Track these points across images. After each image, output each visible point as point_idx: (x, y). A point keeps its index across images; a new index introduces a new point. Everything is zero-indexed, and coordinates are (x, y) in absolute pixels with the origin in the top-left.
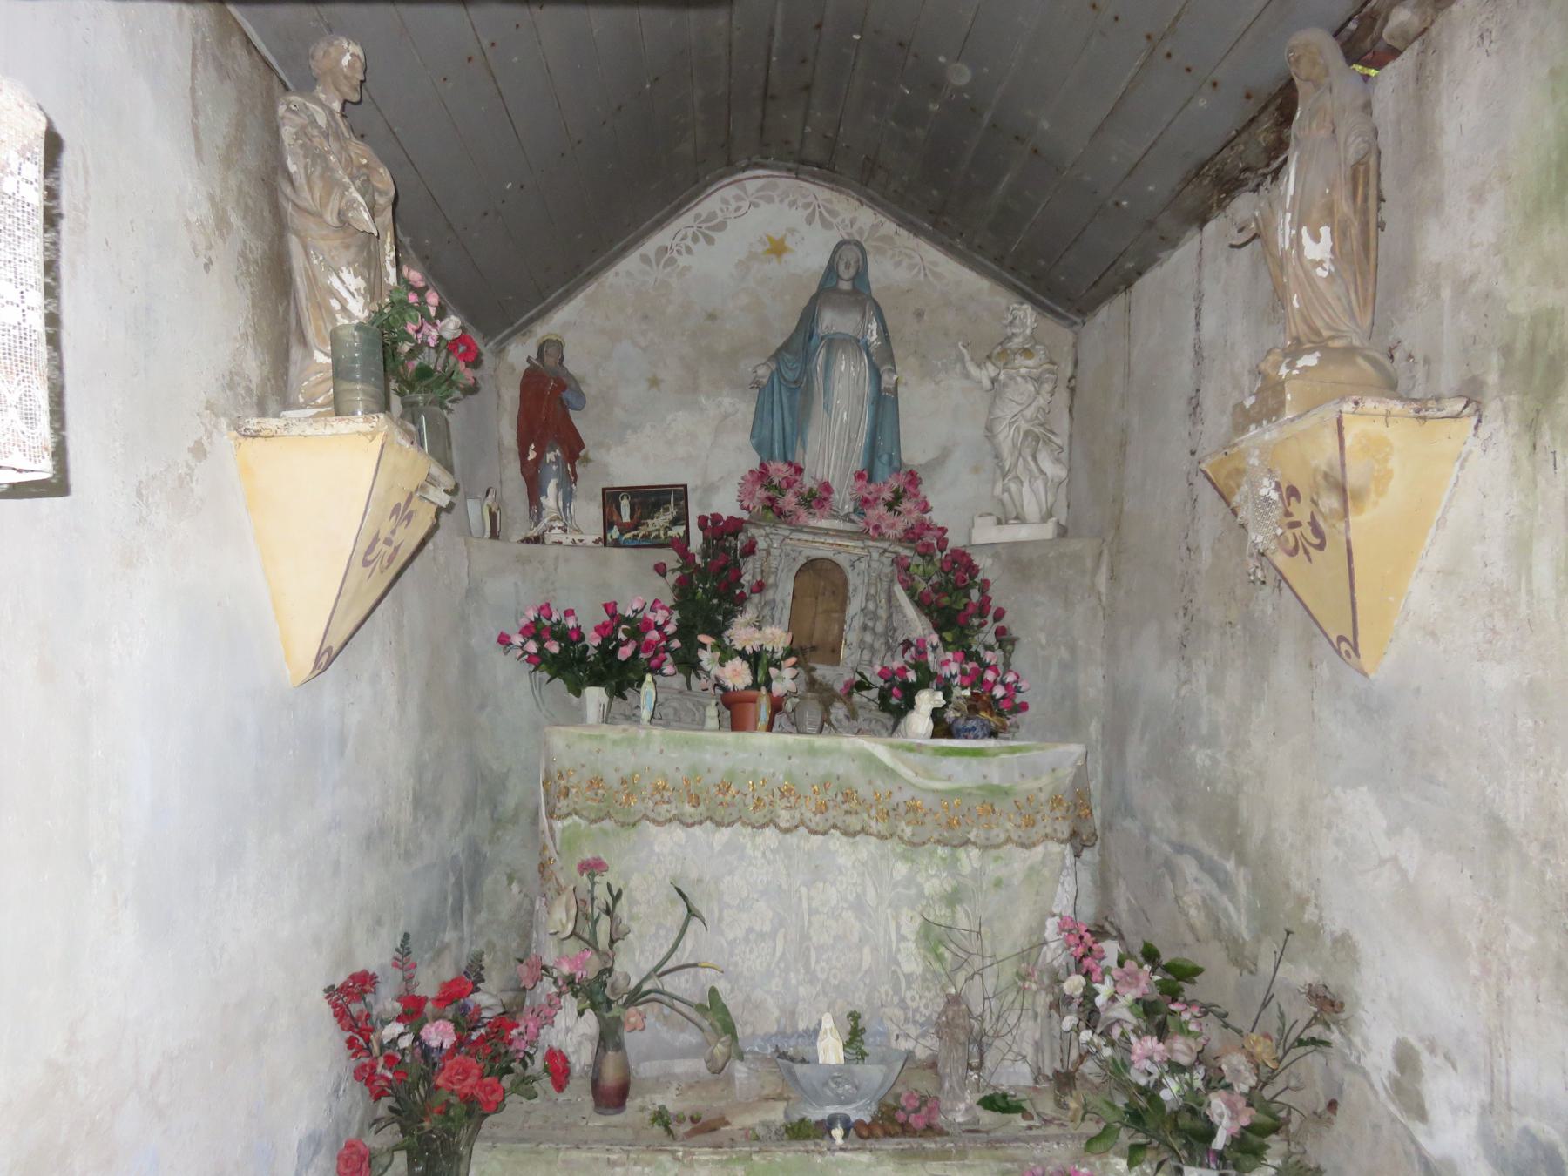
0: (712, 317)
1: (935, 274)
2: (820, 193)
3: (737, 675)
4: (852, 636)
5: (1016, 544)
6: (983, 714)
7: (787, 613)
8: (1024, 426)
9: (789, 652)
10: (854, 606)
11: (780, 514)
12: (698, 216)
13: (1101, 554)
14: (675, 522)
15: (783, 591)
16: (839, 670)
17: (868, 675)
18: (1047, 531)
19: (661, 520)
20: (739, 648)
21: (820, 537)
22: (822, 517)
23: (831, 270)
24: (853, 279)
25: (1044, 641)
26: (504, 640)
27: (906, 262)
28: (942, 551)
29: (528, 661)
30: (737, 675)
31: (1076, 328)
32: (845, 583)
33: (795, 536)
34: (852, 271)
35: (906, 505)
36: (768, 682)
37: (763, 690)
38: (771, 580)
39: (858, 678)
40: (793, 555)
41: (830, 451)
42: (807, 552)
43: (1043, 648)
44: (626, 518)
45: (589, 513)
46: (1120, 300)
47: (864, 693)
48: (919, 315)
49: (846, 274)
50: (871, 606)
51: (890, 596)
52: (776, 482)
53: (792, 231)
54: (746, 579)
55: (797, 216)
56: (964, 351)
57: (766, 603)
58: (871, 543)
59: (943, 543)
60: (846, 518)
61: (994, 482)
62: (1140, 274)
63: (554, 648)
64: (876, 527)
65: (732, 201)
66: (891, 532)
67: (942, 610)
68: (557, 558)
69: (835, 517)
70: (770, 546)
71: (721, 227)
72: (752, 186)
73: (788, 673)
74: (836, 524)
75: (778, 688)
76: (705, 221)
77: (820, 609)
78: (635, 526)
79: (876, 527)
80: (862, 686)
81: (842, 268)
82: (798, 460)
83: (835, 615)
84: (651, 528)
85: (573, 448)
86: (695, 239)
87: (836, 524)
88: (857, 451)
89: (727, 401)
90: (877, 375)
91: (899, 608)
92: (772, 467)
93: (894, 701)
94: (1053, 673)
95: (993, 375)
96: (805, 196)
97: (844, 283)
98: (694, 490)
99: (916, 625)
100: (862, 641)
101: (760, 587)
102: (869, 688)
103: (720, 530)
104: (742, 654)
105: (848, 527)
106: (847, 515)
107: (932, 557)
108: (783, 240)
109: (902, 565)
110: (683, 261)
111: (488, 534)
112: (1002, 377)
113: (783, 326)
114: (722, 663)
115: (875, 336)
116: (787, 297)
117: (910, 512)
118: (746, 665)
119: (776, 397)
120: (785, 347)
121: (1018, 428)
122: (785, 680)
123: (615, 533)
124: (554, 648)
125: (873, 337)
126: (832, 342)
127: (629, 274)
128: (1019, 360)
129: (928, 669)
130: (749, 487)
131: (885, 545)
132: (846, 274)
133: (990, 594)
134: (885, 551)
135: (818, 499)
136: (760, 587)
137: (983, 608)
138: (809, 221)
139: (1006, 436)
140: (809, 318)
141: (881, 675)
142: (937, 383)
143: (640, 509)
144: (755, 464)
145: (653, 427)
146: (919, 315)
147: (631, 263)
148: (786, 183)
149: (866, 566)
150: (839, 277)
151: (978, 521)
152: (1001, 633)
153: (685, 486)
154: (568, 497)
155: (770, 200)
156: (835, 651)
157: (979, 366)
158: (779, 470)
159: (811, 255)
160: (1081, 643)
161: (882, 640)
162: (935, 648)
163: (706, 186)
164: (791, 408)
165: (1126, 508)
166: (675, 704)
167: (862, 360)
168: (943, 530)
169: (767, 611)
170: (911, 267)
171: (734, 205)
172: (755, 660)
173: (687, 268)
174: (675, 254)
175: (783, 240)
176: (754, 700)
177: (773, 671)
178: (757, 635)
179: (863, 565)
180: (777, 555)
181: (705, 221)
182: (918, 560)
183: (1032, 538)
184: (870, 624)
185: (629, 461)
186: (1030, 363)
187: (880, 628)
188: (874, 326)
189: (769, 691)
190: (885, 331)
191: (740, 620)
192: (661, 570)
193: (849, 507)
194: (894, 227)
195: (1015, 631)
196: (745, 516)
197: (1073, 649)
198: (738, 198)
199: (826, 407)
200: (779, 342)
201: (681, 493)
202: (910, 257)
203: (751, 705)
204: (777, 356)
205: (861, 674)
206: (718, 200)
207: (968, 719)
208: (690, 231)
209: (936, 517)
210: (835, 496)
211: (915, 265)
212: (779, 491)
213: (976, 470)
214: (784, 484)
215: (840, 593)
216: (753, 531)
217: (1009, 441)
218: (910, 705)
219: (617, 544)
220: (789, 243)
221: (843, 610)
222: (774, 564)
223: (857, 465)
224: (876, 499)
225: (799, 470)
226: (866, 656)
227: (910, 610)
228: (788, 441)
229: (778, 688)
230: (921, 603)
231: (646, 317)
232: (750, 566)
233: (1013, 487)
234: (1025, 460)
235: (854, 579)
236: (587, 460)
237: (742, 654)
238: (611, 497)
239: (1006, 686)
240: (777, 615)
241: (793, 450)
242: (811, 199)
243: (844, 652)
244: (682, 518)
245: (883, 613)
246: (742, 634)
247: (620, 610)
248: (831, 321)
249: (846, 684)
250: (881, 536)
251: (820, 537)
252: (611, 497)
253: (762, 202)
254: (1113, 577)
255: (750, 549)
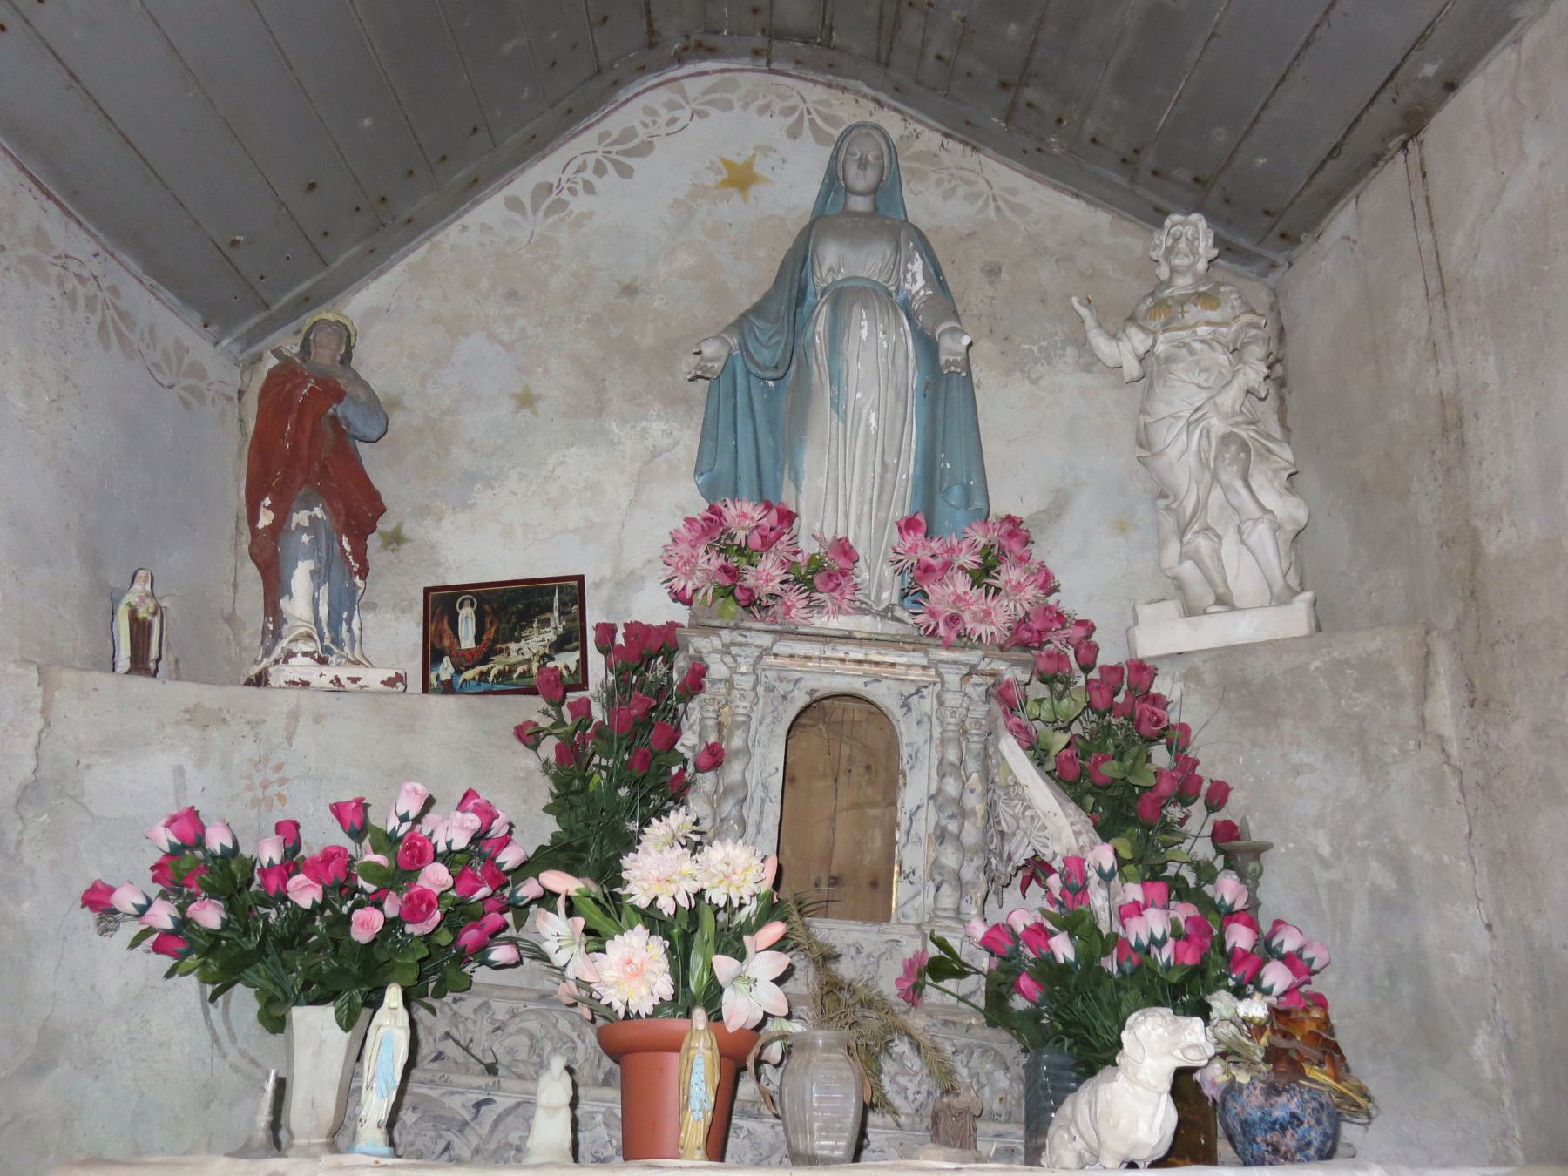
0: (630, 290)
1: (1014, 208)
2: (811, 93)
3: (633, 973)
4: (913, 855)
5: (1231, 652)
6: (1313, 1072)
7: (773, 810)
8: (1218, 426)
9: (771, 909)
10: (914, 791)
11: (752, 603)
12: (603, 136)
13: (1428, 654)
14: (560, 645)
15: (762, 764)
16: (892, 931)
17: (954, 943)
18: (1295, 619)
19: (535, 642)
20: (643, 902)
21: (832, 652)
22: (839, 610)
23: (834, 183)
24: (874, 192)
25: (1326, 851)
26: (98, 900)
27: (962, 190)
28: (1086, 669)
29: (158, 948)
30: (633, 973)
31: (1274, 276)
32: (892, 745)
33: (783, 647)
34: (871, 176)
35: (1009, 574)
36: (712, 996)
37: (699, 1014)
38: (737, 742)
39: (933, 951)
40: (782, 688)
41: (847, 482)
42: (811, 682)
43: (1323, 862)
44: (467, 641)
45: (393, 635)
46: (1395, 171)
47: (949, 984)
48: (993, 271)
49: (861, 180)
50: (951, 787)
51: (988, 758)
52: (741, 536)
53: (765, 150)
54: (688, 742)
55: (773, 128)
56: (1084, 312)
57: (729, 790)
58: (944, 655)
59: (1087, 654)
60: (887, 613)
61: (1161, 545)
62: (1451, 87)
63: (210, 915)
64: (953, 620)
65: (663, 111)
66: (983, 629)
67: (1100, 789)
68: (294, 716)
69: (863, 610)
70: (734, 671)
71: (645, 149)
72: (694, 87)
73: (764, 964)
74: (865, 624)
75: (739, 1009)
76: (614, 143)
77: (843, 802)
78: (484, 654)
79: (953, 620)
80: (945, 966)
81: (852, 170)
82: (788, 499)
83: (877, 812)
84: (514, 658)
85: (359, 512)
86: (600, 170)
87: (865, 624)
88: (899, 489)
89: (657, 427)
90: (928, 346)
91: (1014, 789)
92: (731, 513)
93: (1019, 1003)
94: (1360, 918)
95: (1141, 350)
96: (783, 97)
97: (858, 203)
98: (597, 585)
99: (1057, 825)
100: (936, 865)
101: (714, 758)
102: (961, 972)
103: (646, 648)
104: (652, 919)
105: (892, 628)
106: (890, 608)
107: (1067, 683)
108: (749, 165)
109: (1005, 697)
110: (580, 203)
111: (124, 661)
112: (1161, 348)
113: (750, 278)
114: (595, 938)
115: (920, 282)
116: (762, 254)
117: (1019, 587)
118: (658, 945)
119: (741, 400)
120: (757, 310)
121: (1207, 433)
122: (753, 987)
123: (446, 670)
124: (210, 915)
125: (916, 283)
126: (842, 297)
127: (485, 228)
128: (1193, 312)
129: (1095, 928)
130: (683, 549)
131: (972, 657)
132: (861, 180)
133: (1191, 753)
134: (972, 671)
135: (828, 574)
136: (714, 758)
137: (1186, 790)
138: (794, 133)
139: (1180, 453)
140: (799, 260)
141: (988, 944)
142: (1034, 382)
143: (492, 627)
144: (699, 507)
145: (522, 476)
146: (993, 271)
147: (490, 210)
148: (751, 80)
149: (931, 701)
150: (849, 190)
151: (1146, 612)
152: (1225, 835)
153: (580, 579)
154: (344, 604)
155: (727, 106)
156: (880, 885)
157: (1114, 337)
158: (744, 515)
159: (795, 183)
160: (1416, 850)
161: (978, 861)
162: (1106, 877)
163: (616, 84)
164: (772, 423)
165: (1492, 549)
166: (533, 1025)
167: (898, 323)
168: (1088, 627)
169: (728, 807)
170: (973, 197)
171: (665, 115)
172: (687, 931)
173: (589, 215)
174: (565, 195)
175: (749, 165)
176: (675, 1045)
177: (724, 965)
178: (688, 866)
179: (928, 704)
180: (749, 689)
181: (614, 143)
182: (1039, 690)
183: (1264, 637)
184: (953, 827)
185: (484, 545)
186: (1214, 315)
187: (971, 834)
188: (917, 266)
189: (716, 1017)
190: (938, 272)
191: (657, 830)
192: (529, 736)
193: (889, 596)
194: (938, 138)
195: (1256, 832)
196: (681, 614)
197: (1400, 866)
198: (672, 106)
199: (835, 406)
200: (747, 300)
201: (572, 591)
202: (968, 183)
203: (674, 1055)
204: (741, 324)
205: (941, 944)
206: (637, 110)
207: (1273, 1090)
208: (591, 160)
209: (1072, 601)
210: (862, 574)
211: (978, 196)
212: (748, 562)
213: (1121, 527)
214: (756, 541)
215: (883, 767)
216: (700, 644)
217: (1191, 460)
218: (1094, 1053)
219: (448, 688)
220: (758, 169)
221: (890, 797)
222: (742, 707)
223: (899, 512)
224: (947, 565)
225: (787, 517)
226: (948, 898)
227: (1042, 795)
228: (767, 461)
229: (739, 1009)
230: (1071, 779)
231: (512, 295)
232: (695, 716)
233: (1203, 544)
234: (1226, 489)
235: (910, 734)
236: (396, 539)
237: (652, 919)
238: (440, 605)
239: (1291, 960)
240: (752, 817)
241: (778, 489)
242: (795, 100)
243: (900, 891)
244: (572, 638)
245: (974, 802)
246: (657, 869)
247: (374, 818)
248: (835, 260)
249: (909, 966)
250: (965, 640)
251: (832, 652)
252: (440, 605)
253: (713, 111)
254: (1479, 700)
255: (696, 680)
